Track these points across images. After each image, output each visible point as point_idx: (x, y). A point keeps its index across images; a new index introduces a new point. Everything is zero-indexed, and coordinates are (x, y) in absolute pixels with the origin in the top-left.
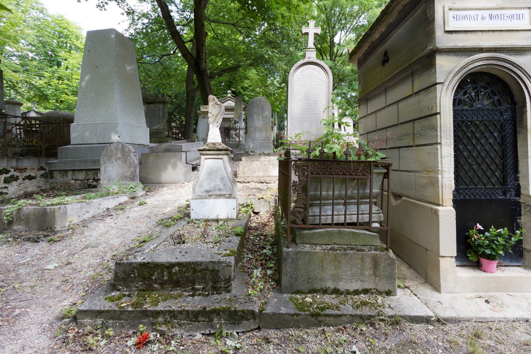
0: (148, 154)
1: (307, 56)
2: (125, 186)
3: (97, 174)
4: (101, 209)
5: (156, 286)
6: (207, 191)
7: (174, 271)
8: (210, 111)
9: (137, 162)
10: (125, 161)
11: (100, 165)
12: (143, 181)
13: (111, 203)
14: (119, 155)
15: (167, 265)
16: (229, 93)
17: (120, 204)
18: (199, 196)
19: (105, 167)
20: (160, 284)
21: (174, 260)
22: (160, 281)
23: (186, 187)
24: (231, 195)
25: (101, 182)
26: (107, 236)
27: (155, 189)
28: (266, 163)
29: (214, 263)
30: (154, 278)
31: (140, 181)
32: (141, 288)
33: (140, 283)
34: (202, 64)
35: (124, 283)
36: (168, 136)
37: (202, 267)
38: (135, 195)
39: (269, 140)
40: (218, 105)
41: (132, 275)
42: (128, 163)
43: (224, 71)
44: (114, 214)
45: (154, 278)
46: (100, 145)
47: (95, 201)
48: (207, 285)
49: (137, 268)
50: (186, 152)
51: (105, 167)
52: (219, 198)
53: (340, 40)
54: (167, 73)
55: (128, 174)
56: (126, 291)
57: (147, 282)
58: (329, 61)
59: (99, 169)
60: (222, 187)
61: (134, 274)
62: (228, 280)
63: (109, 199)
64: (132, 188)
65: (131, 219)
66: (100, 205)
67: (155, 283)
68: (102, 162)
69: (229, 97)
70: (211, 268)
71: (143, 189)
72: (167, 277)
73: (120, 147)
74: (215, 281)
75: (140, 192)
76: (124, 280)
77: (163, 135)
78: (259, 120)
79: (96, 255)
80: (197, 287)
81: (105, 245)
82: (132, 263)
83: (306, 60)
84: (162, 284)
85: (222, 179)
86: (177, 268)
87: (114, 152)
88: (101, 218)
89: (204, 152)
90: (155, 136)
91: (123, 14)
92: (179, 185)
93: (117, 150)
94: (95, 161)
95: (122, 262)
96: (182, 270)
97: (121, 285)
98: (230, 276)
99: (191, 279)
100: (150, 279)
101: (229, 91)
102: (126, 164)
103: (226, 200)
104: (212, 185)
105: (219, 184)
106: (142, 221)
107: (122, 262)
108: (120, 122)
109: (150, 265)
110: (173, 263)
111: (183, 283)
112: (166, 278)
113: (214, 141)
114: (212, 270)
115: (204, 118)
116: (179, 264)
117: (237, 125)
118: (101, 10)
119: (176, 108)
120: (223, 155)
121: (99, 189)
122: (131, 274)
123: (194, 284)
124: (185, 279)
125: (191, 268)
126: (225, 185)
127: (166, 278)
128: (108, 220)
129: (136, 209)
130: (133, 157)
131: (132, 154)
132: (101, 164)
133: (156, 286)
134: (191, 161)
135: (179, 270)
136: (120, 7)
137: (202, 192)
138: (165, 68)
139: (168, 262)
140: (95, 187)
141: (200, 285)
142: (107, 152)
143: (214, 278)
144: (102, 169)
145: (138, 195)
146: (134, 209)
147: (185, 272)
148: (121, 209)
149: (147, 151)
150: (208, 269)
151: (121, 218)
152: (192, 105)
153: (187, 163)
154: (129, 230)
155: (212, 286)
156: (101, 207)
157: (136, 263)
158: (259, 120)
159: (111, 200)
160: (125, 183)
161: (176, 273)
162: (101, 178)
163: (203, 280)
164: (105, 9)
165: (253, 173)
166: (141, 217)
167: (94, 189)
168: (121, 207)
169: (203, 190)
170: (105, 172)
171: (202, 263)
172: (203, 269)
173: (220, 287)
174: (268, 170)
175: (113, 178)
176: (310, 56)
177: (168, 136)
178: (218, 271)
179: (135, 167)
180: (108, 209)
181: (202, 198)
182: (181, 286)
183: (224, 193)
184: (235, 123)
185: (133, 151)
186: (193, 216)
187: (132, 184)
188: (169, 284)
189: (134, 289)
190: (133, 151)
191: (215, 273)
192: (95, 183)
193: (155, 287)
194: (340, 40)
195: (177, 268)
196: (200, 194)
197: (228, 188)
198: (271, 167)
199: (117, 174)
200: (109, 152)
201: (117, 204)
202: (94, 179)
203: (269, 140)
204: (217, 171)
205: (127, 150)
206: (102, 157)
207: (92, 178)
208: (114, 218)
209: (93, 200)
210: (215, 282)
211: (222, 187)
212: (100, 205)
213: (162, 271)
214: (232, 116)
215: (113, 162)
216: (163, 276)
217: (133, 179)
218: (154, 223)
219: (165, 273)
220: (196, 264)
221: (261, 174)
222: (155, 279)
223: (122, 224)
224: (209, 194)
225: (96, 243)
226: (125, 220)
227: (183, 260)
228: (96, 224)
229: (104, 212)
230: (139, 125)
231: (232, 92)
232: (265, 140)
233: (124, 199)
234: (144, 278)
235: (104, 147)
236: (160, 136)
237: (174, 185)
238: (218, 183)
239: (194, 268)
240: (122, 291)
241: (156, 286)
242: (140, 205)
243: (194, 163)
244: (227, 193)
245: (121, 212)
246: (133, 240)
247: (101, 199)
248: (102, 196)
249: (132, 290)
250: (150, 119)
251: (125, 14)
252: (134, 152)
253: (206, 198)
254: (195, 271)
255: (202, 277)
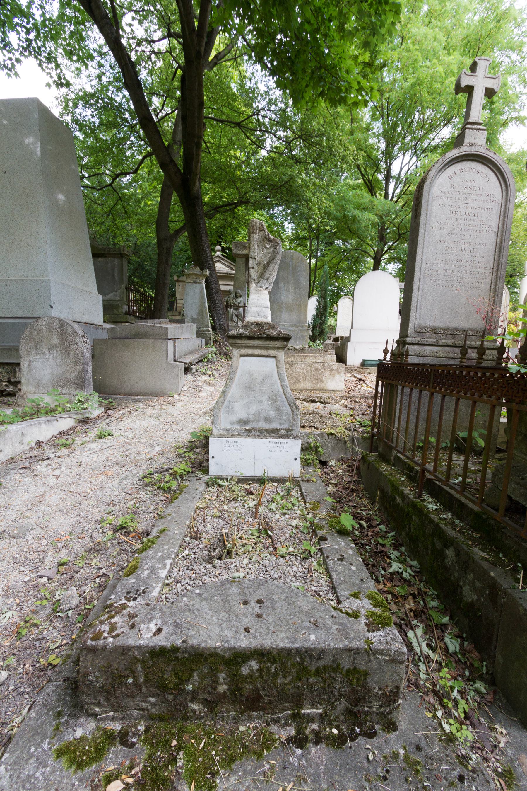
0: (106, 340)
1: (467, 141)
2: (67, 397)
3: (15, 372)
4: (26, 443)
5: (195, 707)
6: (241, 422)
7: (245, 670)
8: (252, 254)
9: (88, 354)
10: (66, 352)
11: (19, 356)
12: (101, 389)
13: (43, 430)
14: (55, 340)
15: (227, 655)
16: (218, 251)
17: (60, 433)
18: (226, 430)
19: (30, 361)
20: (206, 702)
21: (244, 642)
22: (206, 696)
23: (179, 405)
24: (291, 430)
25: (24, 388)
26: (42, 508)
27: (120, 405)
28: (319, 366)
29: (357, 652)
30: (190, 687)
31: (95, 389)
32: (154, 711)
33: (153, 700)
34: (195, 183)
35: (107, 700)
36: (128, 313)
37: (322, 663)
38: (87, 415)
39: (302, 327)
40: (270, 241)
41: (130, 681)
42: (72, 356)
43: (217, 209)
44: (52, 456)
45: (190, 687)
46: (18, 321)
47: (14, 428)
48: (334, 708)
49: (143, 662)
50: (174, 340)
51: (30, 361)
52: (265, 437)
53: (401, 169)
54: (124, 207)
55: (73, 376)
56: (113, 719)
57: (170, 698)
58: (189, 280)
59: (18, 364)
60: (272, 414)
61: (135, 678)
62: (391, 697)
63: (40, 424)
64: (80, 401)
65: (88, 469)
66: (23, 435)
67: (192, 701)
68: (23, 351)
69: (218, 256)
70: (346, 665)
71: (101, 405)
72: (226, 687)
73: (56, 324)
74: (358, 696)
75: (96, 412)
76: (109, 692)
77: (120, 310)
78: (288, 291)
79: (22, 559)
80: (307, 711)
81: (38, 531)
82: (129, 648)
83: (464, 150)
84: (211, 705)
85: (274, 399)
86: (254, 664)
87: (46, 334)
88: (27, 464)
89: (239, 341)
90: (110, 311)
91: (48, 85)
92: (164, 399)
93: (50, 331)
94: (10, 350)
95: (101, 642)
96: (269, 669)
97: (99, 704)
98: (397, 688)
99: (292, 691)
100: (179, 690)
101: (218, 247)
102: (69, 357)
103: (281, 440)
104: (253, 409)
105: (267, 407)
106: (110, 473)
107: (101, 642)
108: (52, 279)
109: (179, 655)
110: (244, 649)
111: (270, 703)
112: (222, 688)
113: (259, 320)
114: (348, 671)
115: (195, 282)
116: (260, 654)
117: (240, 299)
118: (9, 76)
119: (136, 269)
120: (279, 348)
121: (20, 401)
122: (128, 677)
123: (299, 703)
124: (275, 693)
125: (293, 665)
126: (278, 410)
127: (222, 688)
128: (41, 468)
129: (93, 446)
130: (80, 344)
131: (79, 340)
132: (22, 355)
133: (195, 707)
134: (181, 357)
135: (260, 670)
136: (44, 70)
137: (232, 423)
138: (120, 198)
139: (229, 649)
140: (11, 394)
141: (313, 707)
142: (31, 333)
143: (353, 691)
144: (24, 364)
145: (92, 416)
146: (89, 445)
147: (275, 675)
148: (65, 446)
149: (104, 335)
150: (337, 668)
151: (68, 462)
152: (167, 263)
153: (175, 361)
154: (87, 495)
155: (347, 709)
156: (27, 439)
157: (139, 647)
158: (288, 291)
159: (43, 426)
160: (67, 392)
161: (250, 676)
162: (23, 381)
163: (326, 696)
164: (16, 74)
165: (294, 383)
166: (107, 463)
167: (10, 400)
168: (62, 441)
169: (234, 418)
170: (30, 370)
171: (323, 651)
172: (325, 668)
173: (367, 713)
174: (321, 379)
175: (44, 382)
176: (473, 141)
177: (128, 313)
178: (366, 674)
179: (86, 364)
180: (39, 443)
181: (232, 436)
182: (264, 709)
183: (274, 425)
184: (237, 297)
185: (81, 333)
186: (214, 470)
187: (80, 395)
188: (233, 703)
189: (136, 713)
190: (81, 333)
191: (357, 677)
192: (11, 389)
193: (194, 711)
194: (401, 169)
195: (254, 664)
196: (229, 427)
197: (284, 418)
198: (327, 374)
199: (52, 374)
200: (35, 333)
201: (56, 433)
202: (9, 381)
203: (302, 327)
204: (263, 381)
205: (70, 331)
206: (22, 342)
207: (6, 379)
208: (53, 464)
209: (9, 427)
210: (356, 702)
211: (272, 414)
212: (23, 435)
213: (214, 672)
214: (231, 288)
215: (43, 353)
216: (216, 682)
217: (81, 385)
218: (135, 480)
219: (222, 676)
220: (307, 654)
221: (308, 385)
222: (194, 691)
223: (70, 480)
224: (250, 429)
225: (21, 527)
226: (75, 470)
227: (269, 642)
228: (17, 477)
229: (32, 449)
230: (86, 289)
231: (223, 247)
232: (297, 326)
233: (66, 423)
234: (163, 688)
235: (26, 325)
236: (115, 311)
237: (155, 398)
238: (266, 406)
239: (301, 664)
240: (103, 720)
241: (196, 707)
242: (100, 438)
243: (188, 361)
244: (283, 427)
245: (64, 451)
246: (98, 522)
247: (24, 424)
248: (24, 417)
249: (130, 717)
250: (103, 283)
251: (54, 87)
252: (83, 336)
253: (239, 435)
254: (302, 672)
255: (323, 689)
